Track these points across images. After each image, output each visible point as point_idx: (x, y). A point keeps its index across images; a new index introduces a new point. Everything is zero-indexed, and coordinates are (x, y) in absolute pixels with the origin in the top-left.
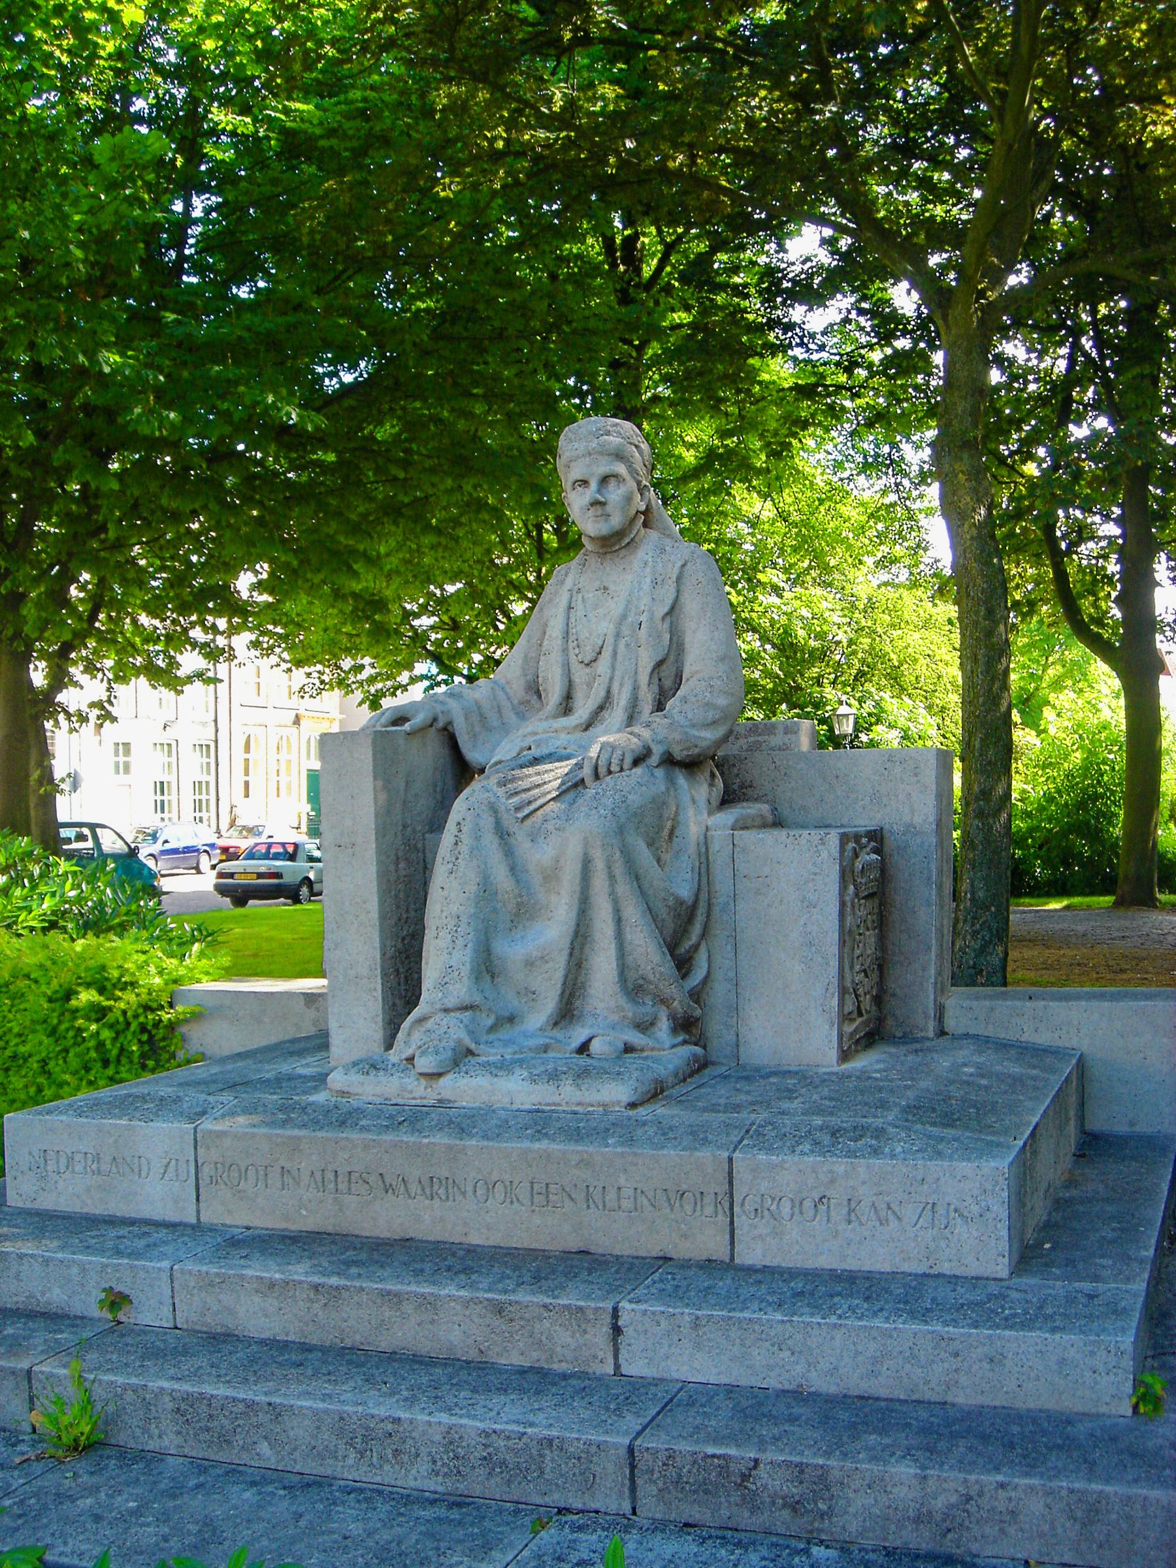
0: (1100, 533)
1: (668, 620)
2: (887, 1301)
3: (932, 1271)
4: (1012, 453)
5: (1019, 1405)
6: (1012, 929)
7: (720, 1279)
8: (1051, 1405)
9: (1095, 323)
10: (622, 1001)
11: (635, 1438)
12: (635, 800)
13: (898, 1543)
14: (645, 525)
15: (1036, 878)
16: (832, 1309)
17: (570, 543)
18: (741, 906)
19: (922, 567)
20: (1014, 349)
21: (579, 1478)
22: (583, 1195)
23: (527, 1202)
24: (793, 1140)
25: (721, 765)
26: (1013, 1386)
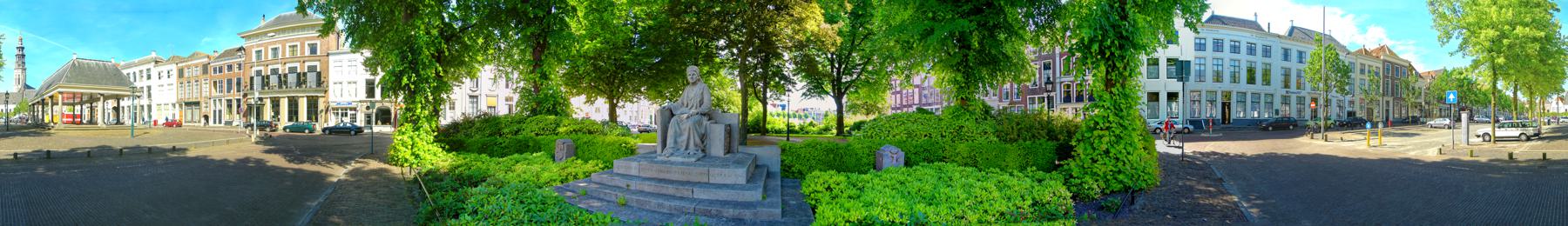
7: (707, 185)
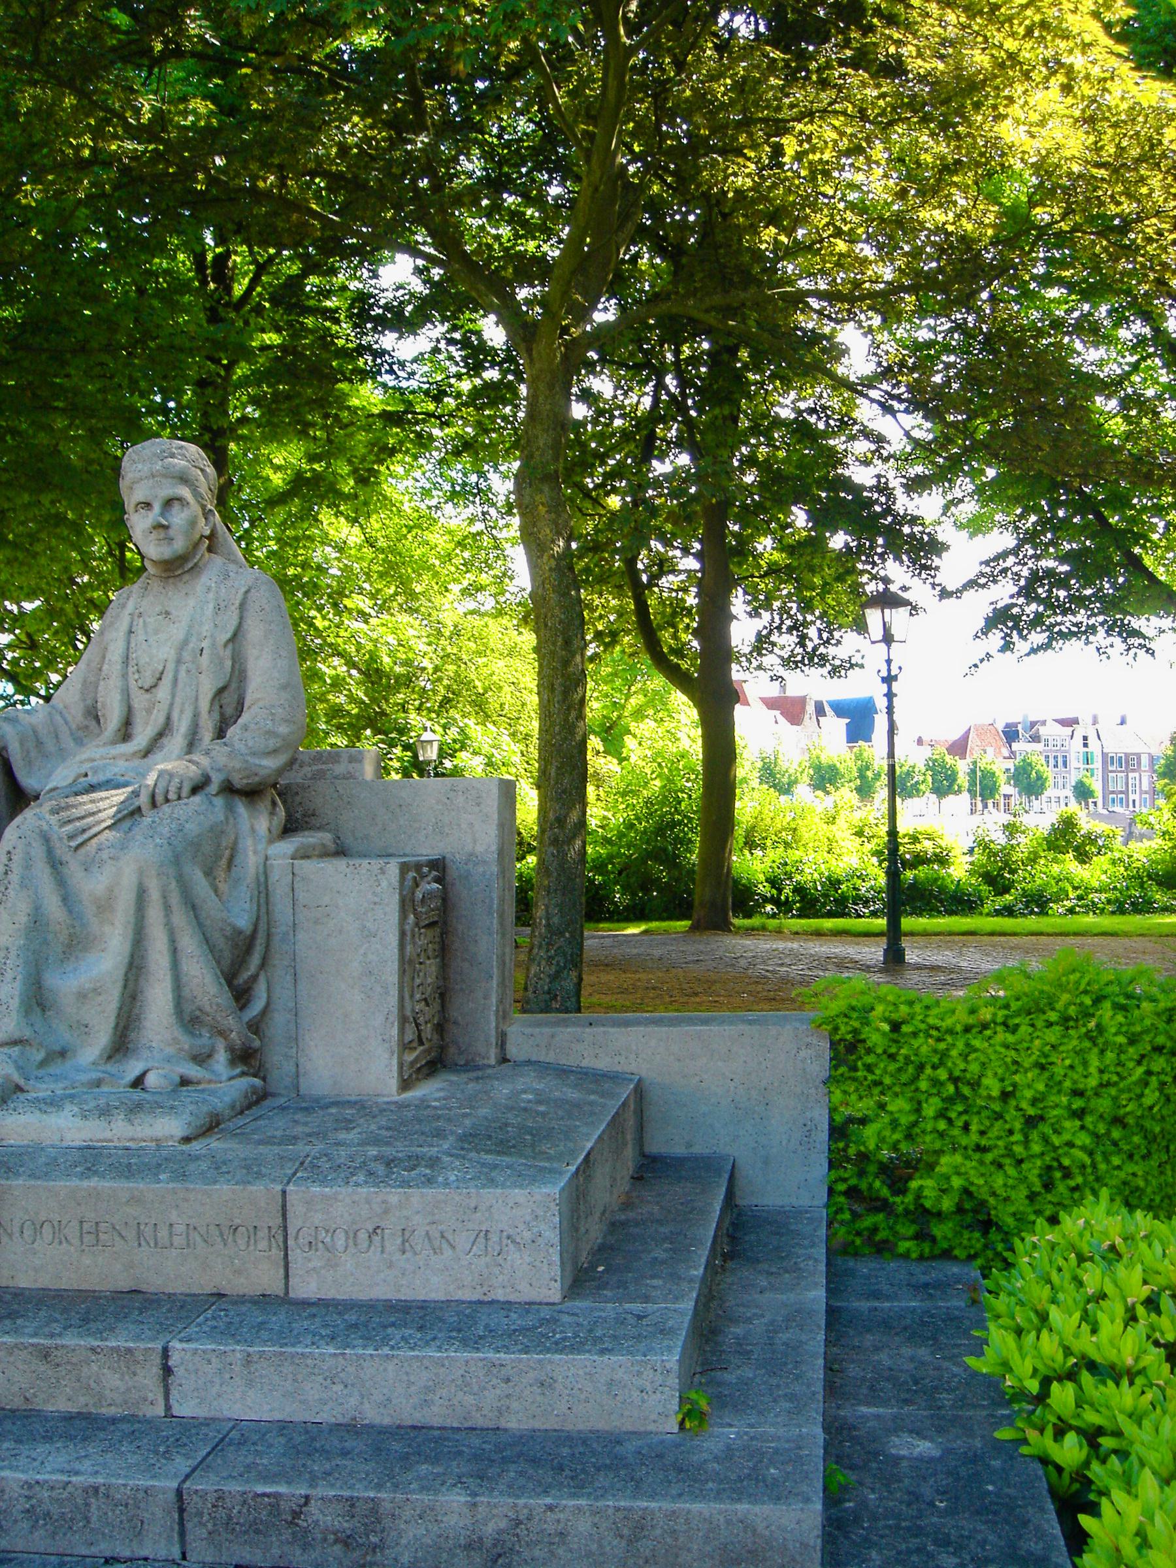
0: (681, 567)
1: (230, 646)
2: (440, 1330)
3: (486, 1299)
5: (569, 1427)
8: (601, 1426)
9: (677, 362)
10: (178, 1033)
11: (184, 1481)
12: (192, 828)
14: (210, 549)
16: (385, 1341)
18: (301, 935)
19: (507, 595)
20: (603, 385)
21: (127, 1526)
22: (134, 1233)
23: (76, 1242)
24: (346, 1172)
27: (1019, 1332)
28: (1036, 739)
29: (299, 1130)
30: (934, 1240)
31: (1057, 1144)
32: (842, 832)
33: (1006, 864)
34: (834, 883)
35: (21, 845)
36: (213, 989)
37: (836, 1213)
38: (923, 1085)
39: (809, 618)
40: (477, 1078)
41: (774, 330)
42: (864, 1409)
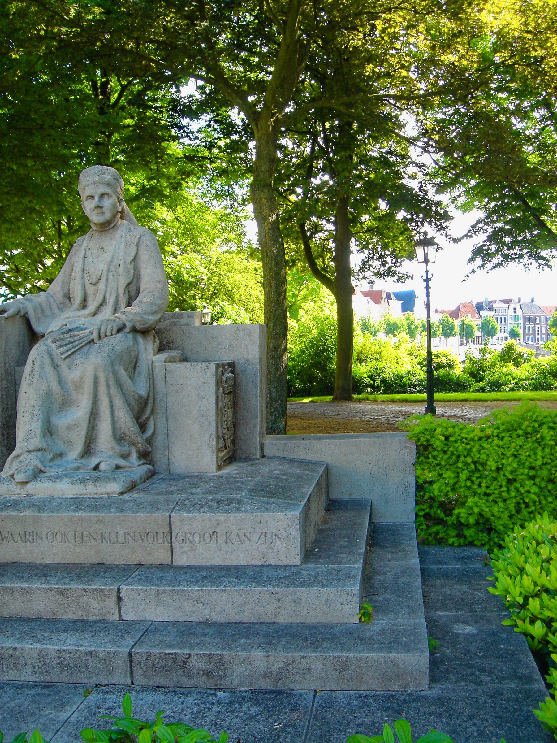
0: (325, 229)
1: (133, 263)
2: (246, 578)
3: (266, 564)
4: (285, 191)
6: (288, 411)
8: (323, 620)
10: (114, 444)
11: (132, 648)
12: (118, 348)
13: (256, 687)
15: (296, 388)
16: (221, 583)
17: (84, 227)
18: (169, 398)
19: (243, 243)
23: (73, 541)
24: (198, 506)
25: (159, 333)
26: (306, 612)
27: (510, 576)
28: (491, 309)
29: (173, 488)
30: (465, 537)
31: (523, 491)
32: (403, 353)
33: (481, 367)
34: (400, 377)
35: (39, 358)
36: (130, 424)
37: (419, 525)
38: (460, 465)
39: (387, 253)
40: (252, 465)
41: (372, 114)
42: (440, 613)
